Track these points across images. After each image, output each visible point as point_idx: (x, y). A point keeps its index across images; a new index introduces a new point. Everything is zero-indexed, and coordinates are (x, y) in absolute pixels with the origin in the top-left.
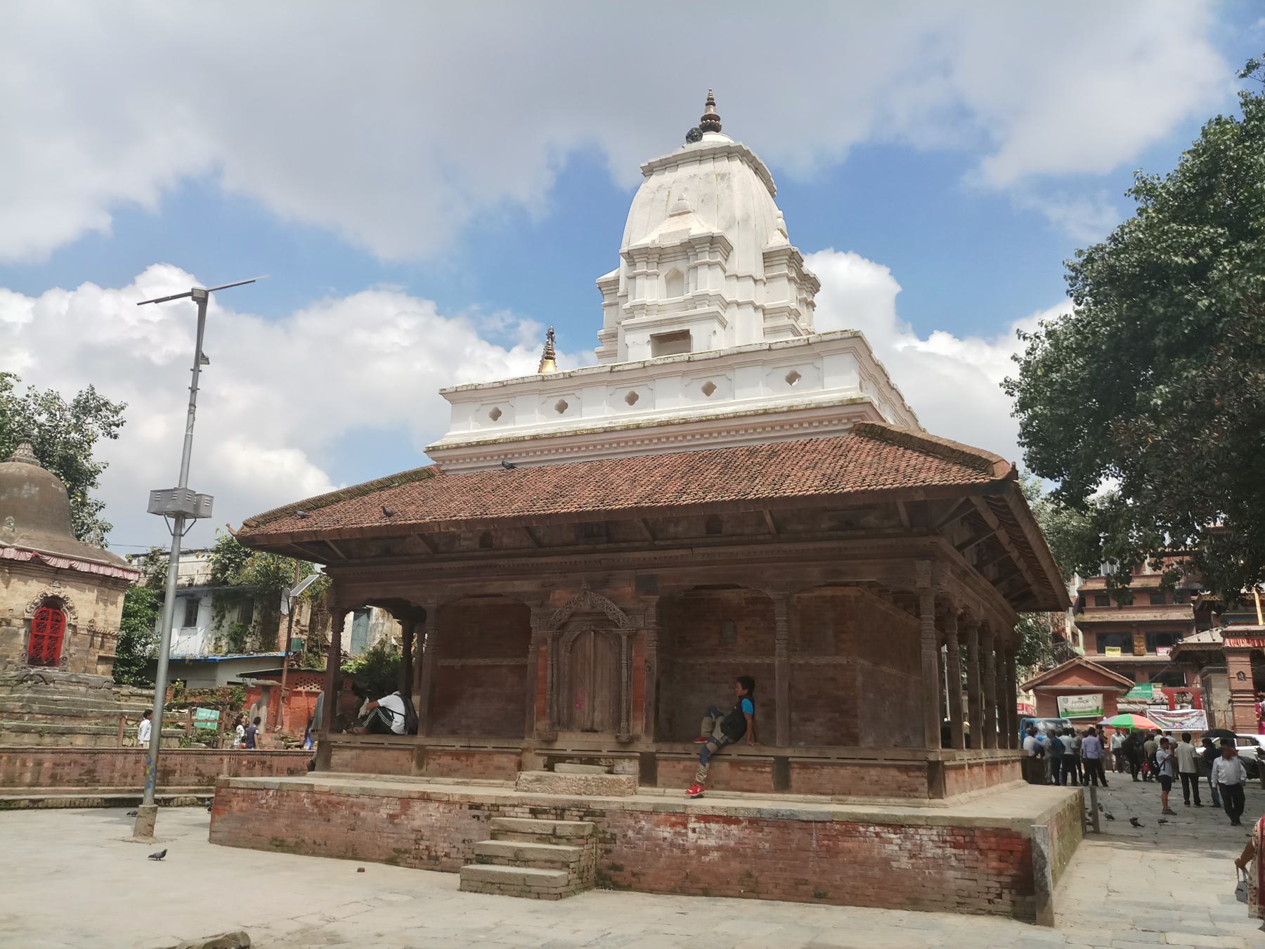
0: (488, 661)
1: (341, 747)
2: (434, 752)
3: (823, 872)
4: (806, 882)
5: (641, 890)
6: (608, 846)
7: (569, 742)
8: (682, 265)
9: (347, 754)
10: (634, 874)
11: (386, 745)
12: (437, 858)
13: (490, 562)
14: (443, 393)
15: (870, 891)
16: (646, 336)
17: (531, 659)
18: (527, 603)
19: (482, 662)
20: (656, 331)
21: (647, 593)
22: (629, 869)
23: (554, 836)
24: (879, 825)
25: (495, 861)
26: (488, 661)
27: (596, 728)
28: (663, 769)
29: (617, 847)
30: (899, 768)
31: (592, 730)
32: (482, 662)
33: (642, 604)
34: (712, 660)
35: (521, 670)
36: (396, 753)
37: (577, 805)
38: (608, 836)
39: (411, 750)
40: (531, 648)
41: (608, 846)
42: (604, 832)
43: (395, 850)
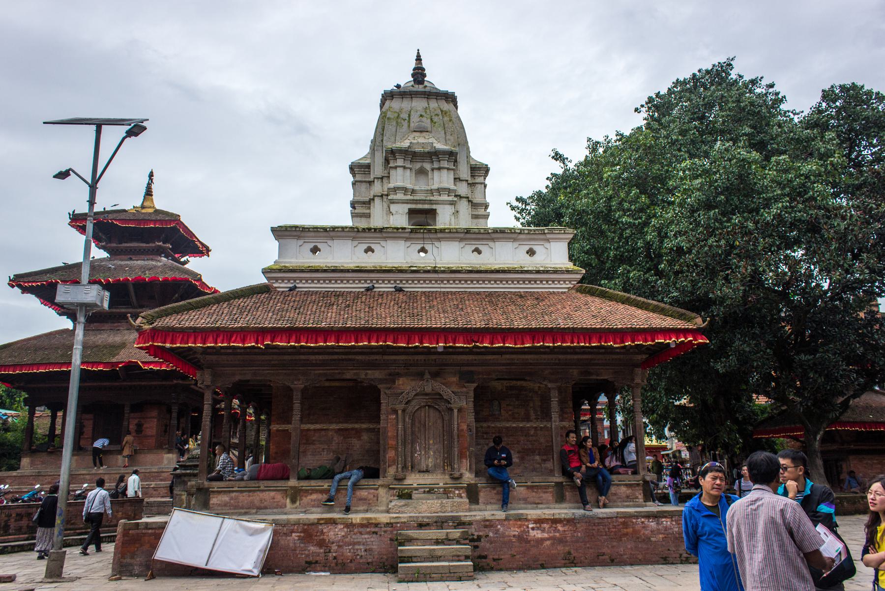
0: (318, 426)
1: (219, 492)
2: (307, 491)
3: (613, 547)
4: (604, 554)
5: (501, 570)
6: (476, 544)
7: (413, 480)
8: (427, 166)
9: (225, 498)
10: (494, 560)
11: (262, 488)
12: (344, 564)
13: (350, 357)
14: (55, 177)
15: (640, 557)
16: (406, 208)
17: (383, 424)
18: (379, 386)
19: (312, 427)
20: (413, 206)
21: (468, 382)
22: (491, 557)
23: (447, 541)
24: (643, 517)
25: (414, 559)
26: (318, 426)
27: (430, 469)
28: (482, 496)
29: (483, 543)
30: (626, 485)
31: (427, 471)
32: (312, 427)
33: (465, 389)
34: (485, 425)
35: (376, 432)
36: (272, 494)
37: (453, 518)
38: (475, 537)
39: (286, 490)
40: (382, 417)
41: (476, 544)
42: (473, 535)
43: (307, 562)
